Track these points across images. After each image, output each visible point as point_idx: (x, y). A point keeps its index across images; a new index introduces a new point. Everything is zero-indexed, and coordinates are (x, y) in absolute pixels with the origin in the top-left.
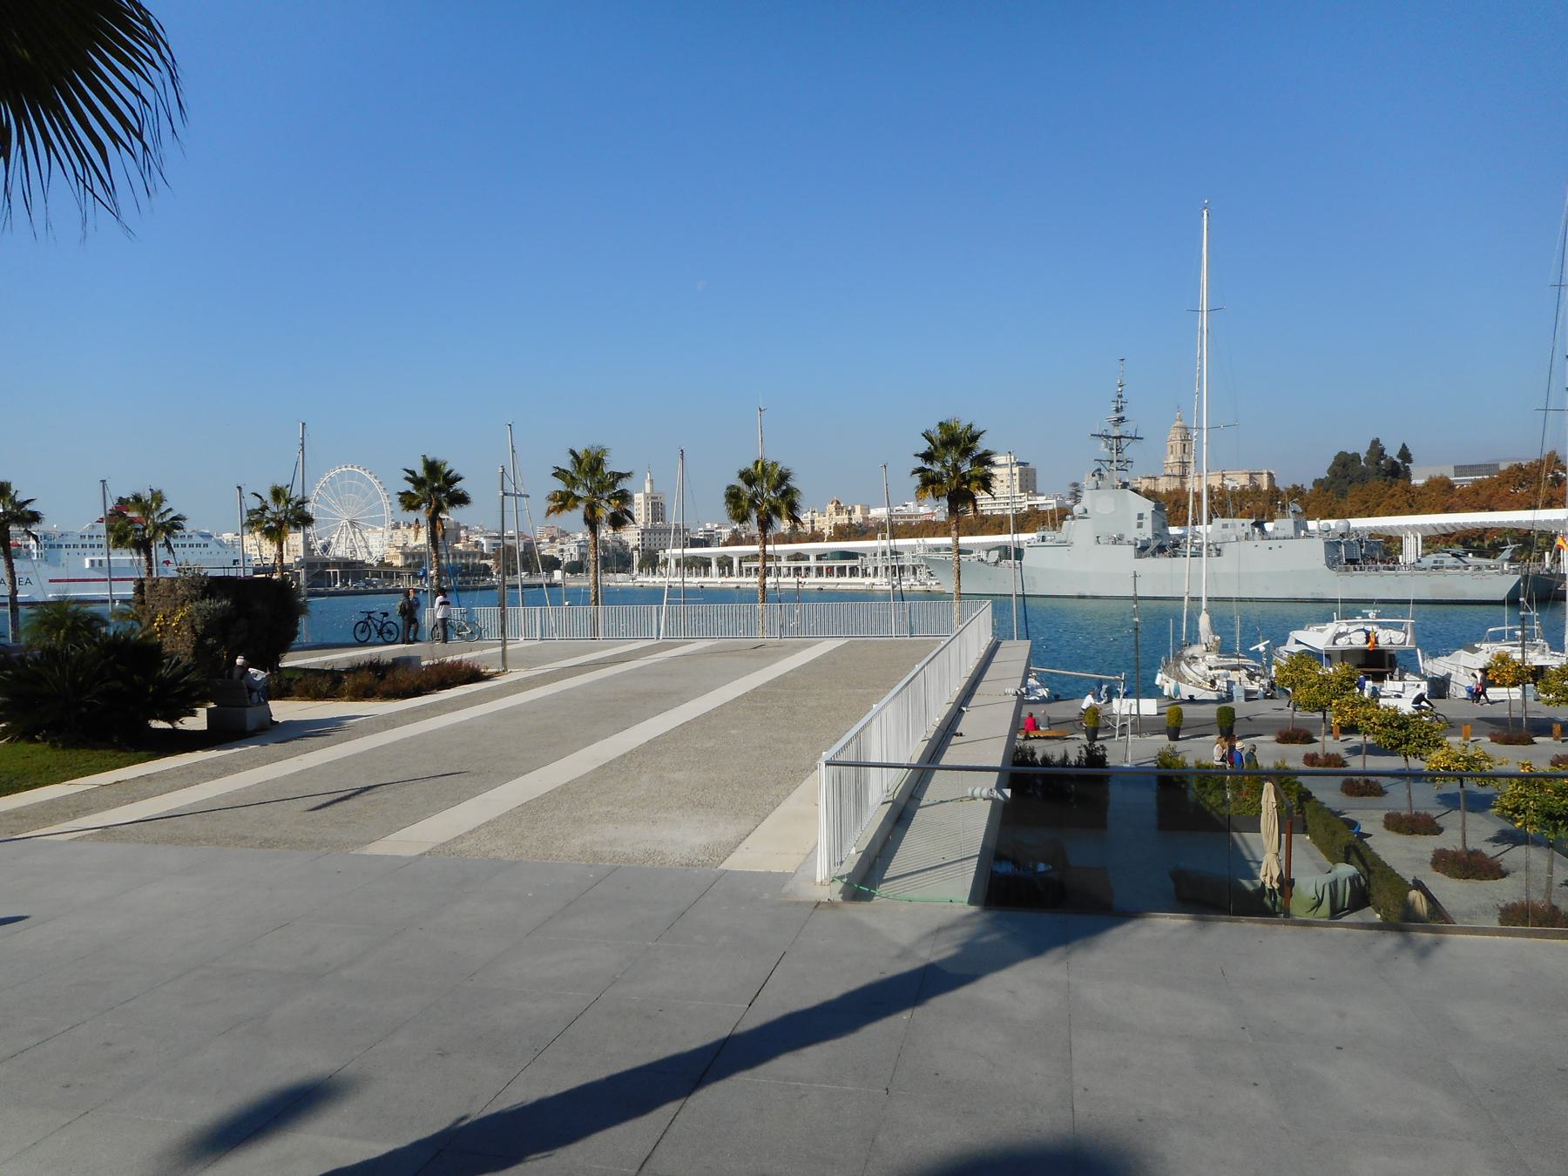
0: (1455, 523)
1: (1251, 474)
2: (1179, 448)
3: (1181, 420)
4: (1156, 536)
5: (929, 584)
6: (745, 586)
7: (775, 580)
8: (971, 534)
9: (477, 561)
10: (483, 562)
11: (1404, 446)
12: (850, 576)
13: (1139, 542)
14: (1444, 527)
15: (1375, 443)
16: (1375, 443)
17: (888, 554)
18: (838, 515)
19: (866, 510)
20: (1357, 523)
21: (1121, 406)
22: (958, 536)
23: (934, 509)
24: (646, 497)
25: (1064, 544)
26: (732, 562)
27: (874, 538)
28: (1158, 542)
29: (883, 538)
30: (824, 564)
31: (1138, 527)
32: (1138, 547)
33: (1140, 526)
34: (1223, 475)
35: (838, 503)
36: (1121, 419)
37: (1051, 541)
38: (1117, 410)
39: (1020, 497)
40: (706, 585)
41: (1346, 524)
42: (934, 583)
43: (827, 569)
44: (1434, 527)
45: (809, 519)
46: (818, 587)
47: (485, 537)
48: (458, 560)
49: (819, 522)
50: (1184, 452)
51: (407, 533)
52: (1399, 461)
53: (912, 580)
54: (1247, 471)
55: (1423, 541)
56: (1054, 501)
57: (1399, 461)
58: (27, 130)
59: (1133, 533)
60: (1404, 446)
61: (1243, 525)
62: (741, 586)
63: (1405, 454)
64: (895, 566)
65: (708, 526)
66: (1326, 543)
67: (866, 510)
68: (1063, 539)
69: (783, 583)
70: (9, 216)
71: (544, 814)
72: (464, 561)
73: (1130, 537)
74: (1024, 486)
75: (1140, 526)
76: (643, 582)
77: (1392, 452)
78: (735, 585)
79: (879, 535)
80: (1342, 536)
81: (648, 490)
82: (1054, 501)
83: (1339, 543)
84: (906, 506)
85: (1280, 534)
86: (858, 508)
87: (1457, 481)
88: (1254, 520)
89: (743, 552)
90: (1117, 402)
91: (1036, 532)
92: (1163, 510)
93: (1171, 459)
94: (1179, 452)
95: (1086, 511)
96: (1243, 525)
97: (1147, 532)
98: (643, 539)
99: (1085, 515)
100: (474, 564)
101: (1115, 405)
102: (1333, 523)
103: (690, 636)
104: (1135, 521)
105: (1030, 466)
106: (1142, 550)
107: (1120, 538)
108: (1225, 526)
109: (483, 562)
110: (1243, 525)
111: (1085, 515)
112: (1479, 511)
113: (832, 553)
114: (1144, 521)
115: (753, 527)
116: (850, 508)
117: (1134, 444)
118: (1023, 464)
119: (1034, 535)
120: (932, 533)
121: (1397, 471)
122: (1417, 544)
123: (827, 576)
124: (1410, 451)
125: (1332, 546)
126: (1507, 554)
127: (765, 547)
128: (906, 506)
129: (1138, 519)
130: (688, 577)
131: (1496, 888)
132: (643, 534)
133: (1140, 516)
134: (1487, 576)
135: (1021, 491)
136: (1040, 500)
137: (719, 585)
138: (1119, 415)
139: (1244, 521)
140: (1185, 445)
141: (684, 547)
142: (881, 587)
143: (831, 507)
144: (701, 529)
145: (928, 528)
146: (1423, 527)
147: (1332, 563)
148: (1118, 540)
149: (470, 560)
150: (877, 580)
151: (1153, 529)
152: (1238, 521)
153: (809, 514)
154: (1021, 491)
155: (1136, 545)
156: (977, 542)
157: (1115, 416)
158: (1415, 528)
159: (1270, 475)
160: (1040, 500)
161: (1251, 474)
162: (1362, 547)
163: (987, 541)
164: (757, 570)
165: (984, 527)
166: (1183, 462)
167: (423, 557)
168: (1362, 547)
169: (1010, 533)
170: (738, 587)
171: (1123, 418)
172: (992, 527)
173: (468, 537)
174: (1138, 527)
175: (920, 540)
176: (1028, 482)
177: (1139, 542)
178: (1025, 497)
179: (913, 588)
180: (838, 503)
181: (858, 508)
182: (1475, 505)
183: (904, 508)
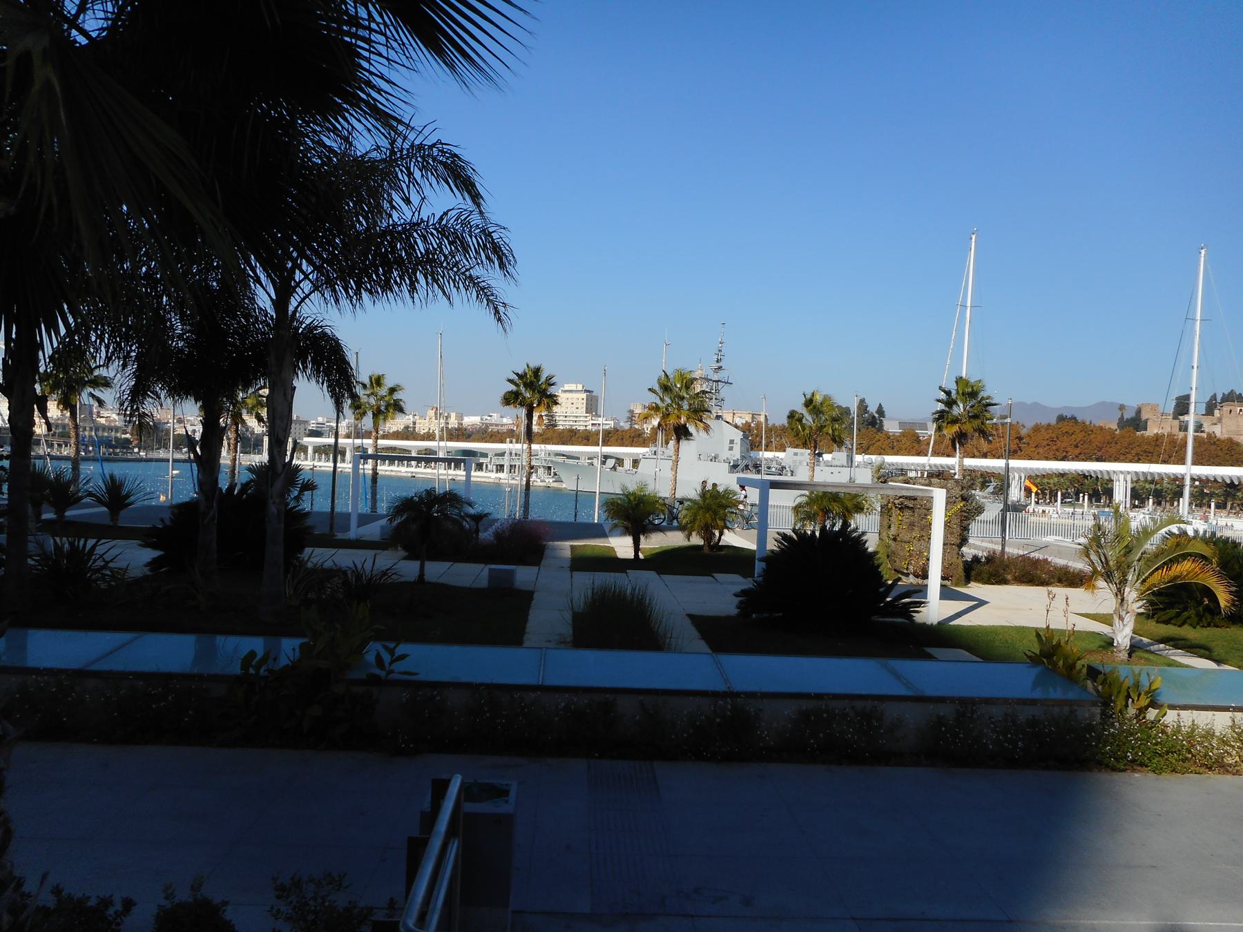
1: (753, 415)
3: (702, 370)
4: (743, 457)
5: (547, 481)
7: (312, 463)
8: (563, 444)
9: (118, 435)
10: (123, 436)
11: (880, 404)
12: (454, 470)
13: (732, 462)
14: (942, 466)
15: (862, 401)
16: (862, 401)
17: (514, 455)
19: (460, 417)
23: (510, 418)
27: (502, 441)
28: (745, 462)
29: (511, 442)
31: (729, 450)
32: (731, 464)
33: (731, 449)
34: (734, 414)
36: (720, 368)
38: (718, 361)
39: (586, 417)
42: (551, 481)
45: (412, 420)
48: (100, 433)
49: (420, 423)
52: (877, 416)
54: (751, 412)
55: (633, 462)
56: (612, 422)
57: (877, 416)
58: (454, 23)
59: (725, 454)
60: (880, 404)
63: (880, 411)
65: (320, 420)
67: (460, 417)
70: (389, 97)
72: (106, 434)
73: (723, 456)
74: (589, 409)
75: (731, 449)
77: (872, 409)
79: (508, 440)
82: (612, 422)
85: (835, 463)
86: (453, 415)
87: (921, 433)
91: (649, 447)
92: (747, 438)
97: (736, 454)
100: (116, 438)
102: (874, 457)
103: (996, 536)
104: (727, 445)
105: (594, 394)
107: (716, 458)
108: (796, 454)
113: (456, 451)
114: (734, 445)
115: (368, 422)
116: (446, 415)
117: (726, 386)
118: (589, 391)
121: (873, 422)
122: (1126, 487)
126: (991, 489)
127: (376, 442)
129: (733, 447)
130: (381, 465)
133: (732, 442)
135: (586, 413)
136: (600, 420)
138: (719, 365)
144: (314, 422)
145: (511, 435)
146: (1025, 469)
148: (715, 459)
149: (113, 433)
151: (741, 452)
154: (586, 413)
155: (730, 463)
156: (580, 450)
157: (716, 365)
159: (766, 416)
160: (600, 420)
161: (753, 415)
163: (500, 447)
165: (573, 439)
167: (67, 428)
169: (599, 445)
171: (721, 367)
172: (580, 439)
174: (729, 450)
175: (543, 446)
176: (592, 406)
177: (732, 462)
178: (590, 418)
181: (453, 415)
183: (489, 418)
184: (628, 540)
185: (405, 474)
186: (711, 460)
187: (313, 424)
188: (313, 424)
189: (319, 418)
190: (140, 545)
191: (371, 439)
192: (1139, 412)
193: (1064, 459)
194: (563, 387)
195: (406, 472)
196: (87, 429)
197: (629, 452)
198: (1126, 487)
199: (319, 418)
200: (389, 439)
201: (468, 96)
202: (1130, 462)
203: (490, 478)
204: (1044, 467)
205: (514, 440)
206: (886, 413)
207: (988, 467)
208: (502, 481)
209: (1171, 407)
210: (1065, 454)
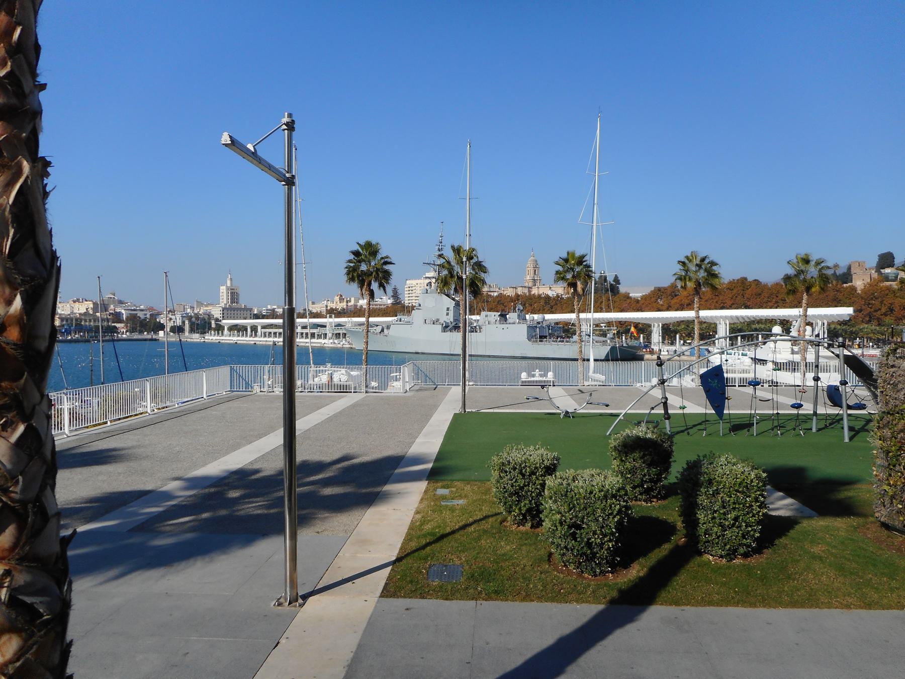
0: (756, 316)
2: (532, 272)
6: (223, 341)
10: (113, 324)
14: (754, 318)
18: (340, 303)
20: (548, 317)
21: (442, 248)
22: (807, 308)
24: (228, 289)
25: (408, 323)
26: (247, 329)
30: (305, 331)
33: (447, 314)
35: (341, 296)
37: (403, 321)
40: (239, 342)
41: (543, 317)
43: (343, 335)
44: (737, 318)
46: (254, 342)
47: (125, 309)
50: (535, 274)
51: (73, 306)
53: (344, 342)
61: (494, 316)
62: (257, 343)
63: (617, 280)
64: (308, 333)
65: (269, 307)
66: (528, 327)
67: (357, 300)
68: (408, 321)
69: (300, 342)
71: (801, 538)
73: (442, 321)
75: (447, 314)
76: (220, 340)
77: (610, 279)
78: (253, 342)
80: (539, 323)
81: (229, 284)
83: (536, 327)
84: (382, 299)
86: (353, 299)
88: (499, 313)
89: (667, 318)
90: (439, 245)
91: (396, 316)
93: (528, 278)
94: (532, 274)
95: (420, 305)
96: (495, 316)
97: (450, 318)
98: (223, 314)
99: (420, 308)
101: (437, 247)
106: (446, 328)
109: (113, 324)
110: (495, 316)
111: (420, 308)
112: (637, 312)
116: (348, 299)
119: (396, 318)
120: (377, 315)
122: (726, 328)
123: (300, 338)
124: (619, 278)
125: (532, 328)
128: (382, 299)
131: (560, 499)
132: (223, 310)
133: (448, 309)
134: (597, 346)
137: (210, 341)
138: (440, 253)
139: (495, 313)
140: (535, 271)
141: (579, 312)
142: (327, 345)
143: (337, 298)
144: (265, 309)
146: (826, 316)
147: (530, 337)
150: (326, 341)
151: (454, 316)
152: (493, 314)
153: (326, 301)
155: (443, 324)
158: (726, 317)
162: (549, 329)
164: (280, 334)
166: (534, 280)
168: (549, 329)
170: (219, 342)
173: (115, 309)
175: (349, 319)
179: (344, 346)
180: (341, 296)
181: (353, 299)
182: (634, 308)
183: (380, 300)
184: (336, 379)
185: (215, 341)
186: (434, 323)
187: (264, 310)
188: (264, 310)
189: (268, 306)
190: (257, 471)
191: (693, 310)
192: (849, 268)
193: (722, 308)
194: (425, 275)
195: (216, 339)
196: (88, 320)
197: (556, 318)
198: (726, 328)
199: (268, 306)
200: (670, 311)
201: (60, 261)
202: (771, 308)
203: (232, 340)
204: (737, 315)
205: (333, 316)
206: (621, 281)
207: (634, 318)
208: (325, 345)
209: (873, 261)
210: (722, 305)
